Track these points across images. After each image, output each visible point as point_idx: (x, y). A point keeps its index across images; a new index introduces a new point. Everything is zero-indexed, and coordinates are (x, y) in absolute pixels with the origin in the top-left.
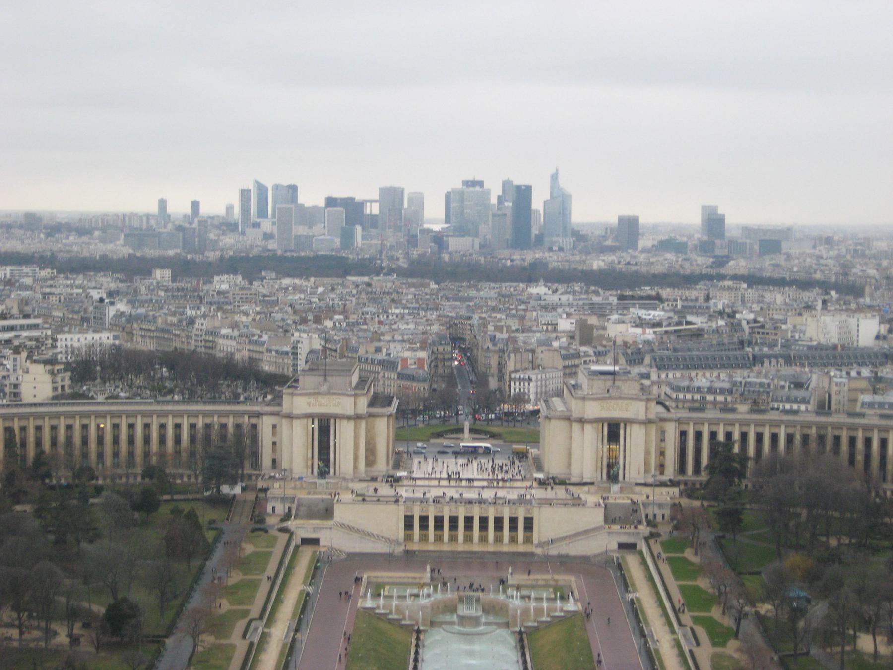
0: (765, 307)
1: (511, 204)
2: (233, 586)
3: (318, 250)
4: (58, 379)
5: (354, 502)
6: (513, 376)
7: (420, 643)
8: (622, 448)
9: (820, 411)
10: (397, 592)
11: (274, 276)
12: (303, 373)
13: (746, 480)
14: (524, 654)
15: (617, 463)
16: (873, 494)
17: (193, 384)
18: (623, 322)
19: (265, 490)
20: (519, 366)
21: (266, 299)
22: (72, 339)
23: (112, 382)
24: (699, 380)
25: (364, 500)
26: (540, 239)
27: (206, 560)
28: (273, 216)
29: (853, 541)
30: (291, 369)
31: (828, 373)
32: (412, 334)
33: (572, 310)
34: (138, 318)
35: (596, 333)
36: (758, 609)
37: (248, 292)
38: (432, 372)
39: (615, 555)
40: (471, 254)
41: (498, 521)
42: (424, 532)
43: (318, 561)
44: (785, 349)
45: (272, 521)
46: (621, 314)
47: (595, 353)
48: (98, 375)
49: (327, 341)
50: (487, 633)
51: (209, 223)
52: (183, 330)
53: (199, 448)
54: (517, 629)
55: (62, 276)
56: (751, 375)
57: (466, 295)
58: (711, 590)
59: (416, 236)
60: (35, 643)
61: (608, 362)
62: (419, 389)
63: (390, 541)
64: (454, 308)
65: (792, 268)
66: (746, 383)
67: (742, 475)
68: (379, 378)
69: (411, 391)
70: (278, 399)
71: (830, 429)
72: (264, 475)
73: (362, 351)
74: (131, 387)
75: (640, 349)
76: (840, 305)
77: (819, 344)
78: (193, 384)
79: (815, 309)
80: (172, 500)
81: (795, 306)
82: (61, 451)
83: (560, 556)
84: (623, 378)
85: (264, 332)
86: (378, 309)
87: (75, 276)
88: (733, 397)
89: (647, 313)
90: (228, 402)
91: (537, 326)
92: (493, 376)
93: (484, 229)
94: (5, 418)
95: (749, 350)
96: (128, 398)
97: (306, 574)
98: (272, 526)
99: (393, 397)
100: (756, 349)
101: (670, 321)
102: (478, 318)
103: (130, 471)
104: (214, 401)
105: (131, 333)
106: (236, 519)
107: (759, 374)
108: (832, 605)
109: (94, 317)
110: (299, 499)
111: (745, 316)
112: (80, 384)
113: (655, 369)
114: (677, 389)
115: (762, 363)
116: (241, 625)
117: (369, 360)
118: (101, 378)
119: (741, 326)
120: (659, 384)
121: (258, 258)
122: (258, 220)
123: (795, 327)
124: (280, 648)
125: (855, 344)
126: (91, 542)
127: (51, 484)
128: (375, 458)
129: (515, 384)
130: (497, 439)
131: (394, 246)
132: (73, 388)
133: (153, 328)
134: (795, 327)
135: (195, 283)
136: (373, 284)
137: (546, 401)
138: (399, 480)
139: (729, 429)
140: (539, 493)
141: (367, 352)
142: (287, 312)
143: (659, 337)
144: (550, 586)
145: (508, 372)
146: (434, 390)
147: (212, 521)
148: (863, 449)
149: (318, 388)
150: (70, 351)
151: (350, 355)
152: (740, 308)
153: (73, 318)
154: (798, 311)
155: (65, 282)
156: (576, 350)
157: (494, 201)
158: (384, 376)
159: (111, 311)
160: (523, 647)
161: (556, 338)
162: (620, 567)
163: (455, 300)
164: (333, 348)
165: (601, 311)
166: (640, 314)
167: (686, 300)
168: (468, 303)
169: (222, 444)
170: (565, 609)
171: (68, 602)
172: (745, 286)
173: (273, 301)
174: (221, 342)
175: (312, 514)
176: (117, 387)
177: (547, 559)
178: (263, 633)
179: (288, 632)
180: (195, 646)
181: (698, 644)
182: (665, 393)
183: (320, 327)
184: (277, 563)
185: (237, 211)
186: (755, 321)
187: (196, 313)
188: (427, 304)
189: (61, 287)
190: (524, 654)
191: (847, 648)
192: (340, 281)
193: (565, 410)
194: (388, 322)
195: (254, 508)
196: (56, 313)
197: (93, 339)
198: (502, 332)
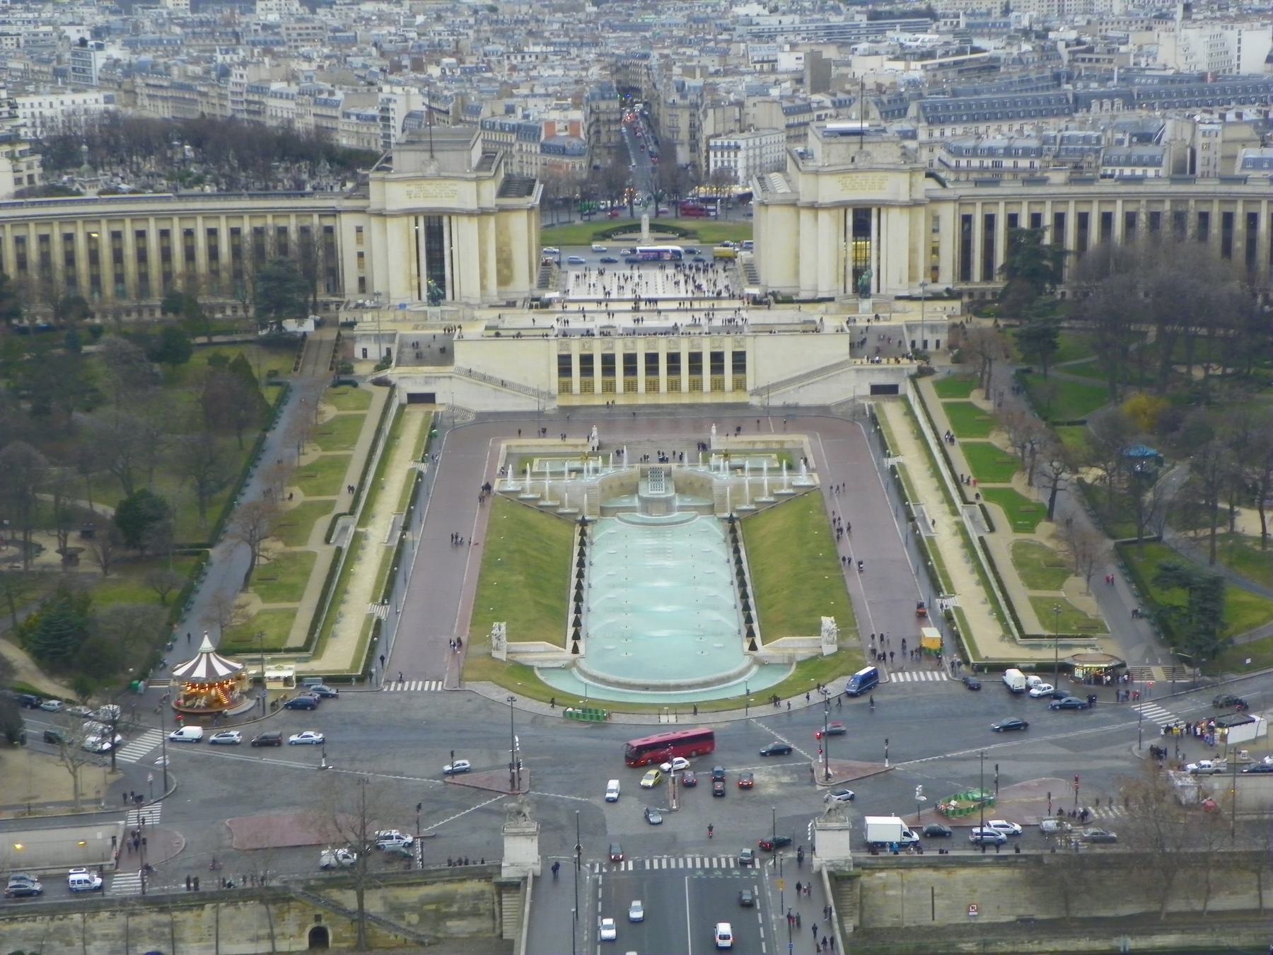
0: (1095, 19)
2: (309, 467)
4: (23, 166)
5: (483, 338)
6: (712, 142)
8: (874, 244)
9: (1177, 176)
10: (550, 468)
12: (397, 147)
13: (1062, 286)
14: (737, 551)
15: (867, 267)
16: (1260, 300)
17: (232, 169)
18: (877, 54)
20: (720, 128)
21: (337, 34)
22: (40, 104)
23: (107, 168)
24: (991, 137)
25: (498, 335)
27: (266, 430)
29: (1229, 371)
30: (381, 142)
31: (1192, 116)
32: (560, 85)
33: (799, 38)
34: (141, 68)
35: (835, 72)
36: (1083, 476)
37: (309, 25)
38: (592, 142)
39: (867, 403)
41: (695, 359)
42: (587, 379)
43: (433, 427)
44: (1124, 84)
45: (362, 369)
46: (872, 42)
47: (834, 103)
48: (85, 158)
49: (433, 98)
50: (682, 522)
52: (212, 86)
53: (248, 265)
54: (727, 515)
55: (19, 6)
56: (1071, 125)
57: (640, 20)
58: (1010, 450)
60: (9, 564)
61: (854, 117)
62: (574, 167)
63: (538, 394)
64: (622, 41)
67: (1056, 278)
68: (514, 152)
69: (561, 171)
71: (1192, 203)
72: (348, 303)
73: (485, 113)
74: (137, 175)
75: (901, 94)
76: (1212, 11)
77: (1178, 73)
78: (232, 169)
79: (1172, 19)
80: (210, 344)
81: (1142, 16)
82: (34, 275)
83: (786, 407)
84: (875, 139)
85: (337, 86)
86: (508, 46)
87: (40, 6)
88: (1043, 161)
89: (913, 37)
90: (288, 195)
91: (747, 66)
92: (682, 144)
95: (1068, 87)
96: (133, 192)
97: (416, 447)
98: (363, 378)
99: (534, 181)
100: (1080, 85)
101: (946, 48)
102: (658, 57)
103: (143, 303)
104: (265, 193)
105: (132, 92)
106: (309, 369)
107: (1083, 123)
108: (1195, 467)
109: (74, 69)
110: (402, 336)
111: (1063, 34)
112: (57, 172)
113: (924, 124)
114: (957, 152)
115: (1089, 108)
116: (322, 523)
117: (497, 127)
118: (90, 163)
119: (1056, 50)
120: (931, 146)
123: (1140, 47)
124: (381, 555)
125: (1235, 71)
126: (88, 410)
127: (21, 325)
128: (512, 272)
129: (715, 156)
130: (689, 238)
132: (48, 179)
133: (165, 84)
134: (1140, 47)
135: (227, 12)
136: (500, 7)
137: (761, 179)
138: (546, 304)
140: (757, 316)
141: (493, 114)
142: (370, 55)
143: (930, 73)
144: (773, 451)
145: (704, 137)
146: (596, 168)
147: (273, 374)
148: (1245, 230)
149: (421, 171)
150: (38, 122)
151: (468, 119)
152: (1055, 23)
153: (40, 72)
154: (1146, 23)
155: (24, 15)
156: (805, 99)
158: (521, 150)
159: (99, 60)
160: (735, 540)
162: (874, 420)
163: (623, 29)
164: (443, 108)
165: (842, 37)
166: (902, 40)
169: (282, 257)
170: (794, 483)
171: (57, 500)
173: (348, 37)
174: (272, 102)
175: (420, 354)
176: (116, 175)
177: (768, 410)
178: (356, 534)
179: (392, 531)
180: (254, 556)
181: (992, 529)
182: (940, 160)
183: (422, 76)
184: (374, 428)
186: (1079, 42)
187: (232, 59)
188: (581, 37)
189: (19, 23)
190: (737, 551)
191: (1220, 530)
193: (789, 191)
194: (523, 66)
195: (335, 351)
196: (13, 64)
197: (73, 102)
198: (694, 78)
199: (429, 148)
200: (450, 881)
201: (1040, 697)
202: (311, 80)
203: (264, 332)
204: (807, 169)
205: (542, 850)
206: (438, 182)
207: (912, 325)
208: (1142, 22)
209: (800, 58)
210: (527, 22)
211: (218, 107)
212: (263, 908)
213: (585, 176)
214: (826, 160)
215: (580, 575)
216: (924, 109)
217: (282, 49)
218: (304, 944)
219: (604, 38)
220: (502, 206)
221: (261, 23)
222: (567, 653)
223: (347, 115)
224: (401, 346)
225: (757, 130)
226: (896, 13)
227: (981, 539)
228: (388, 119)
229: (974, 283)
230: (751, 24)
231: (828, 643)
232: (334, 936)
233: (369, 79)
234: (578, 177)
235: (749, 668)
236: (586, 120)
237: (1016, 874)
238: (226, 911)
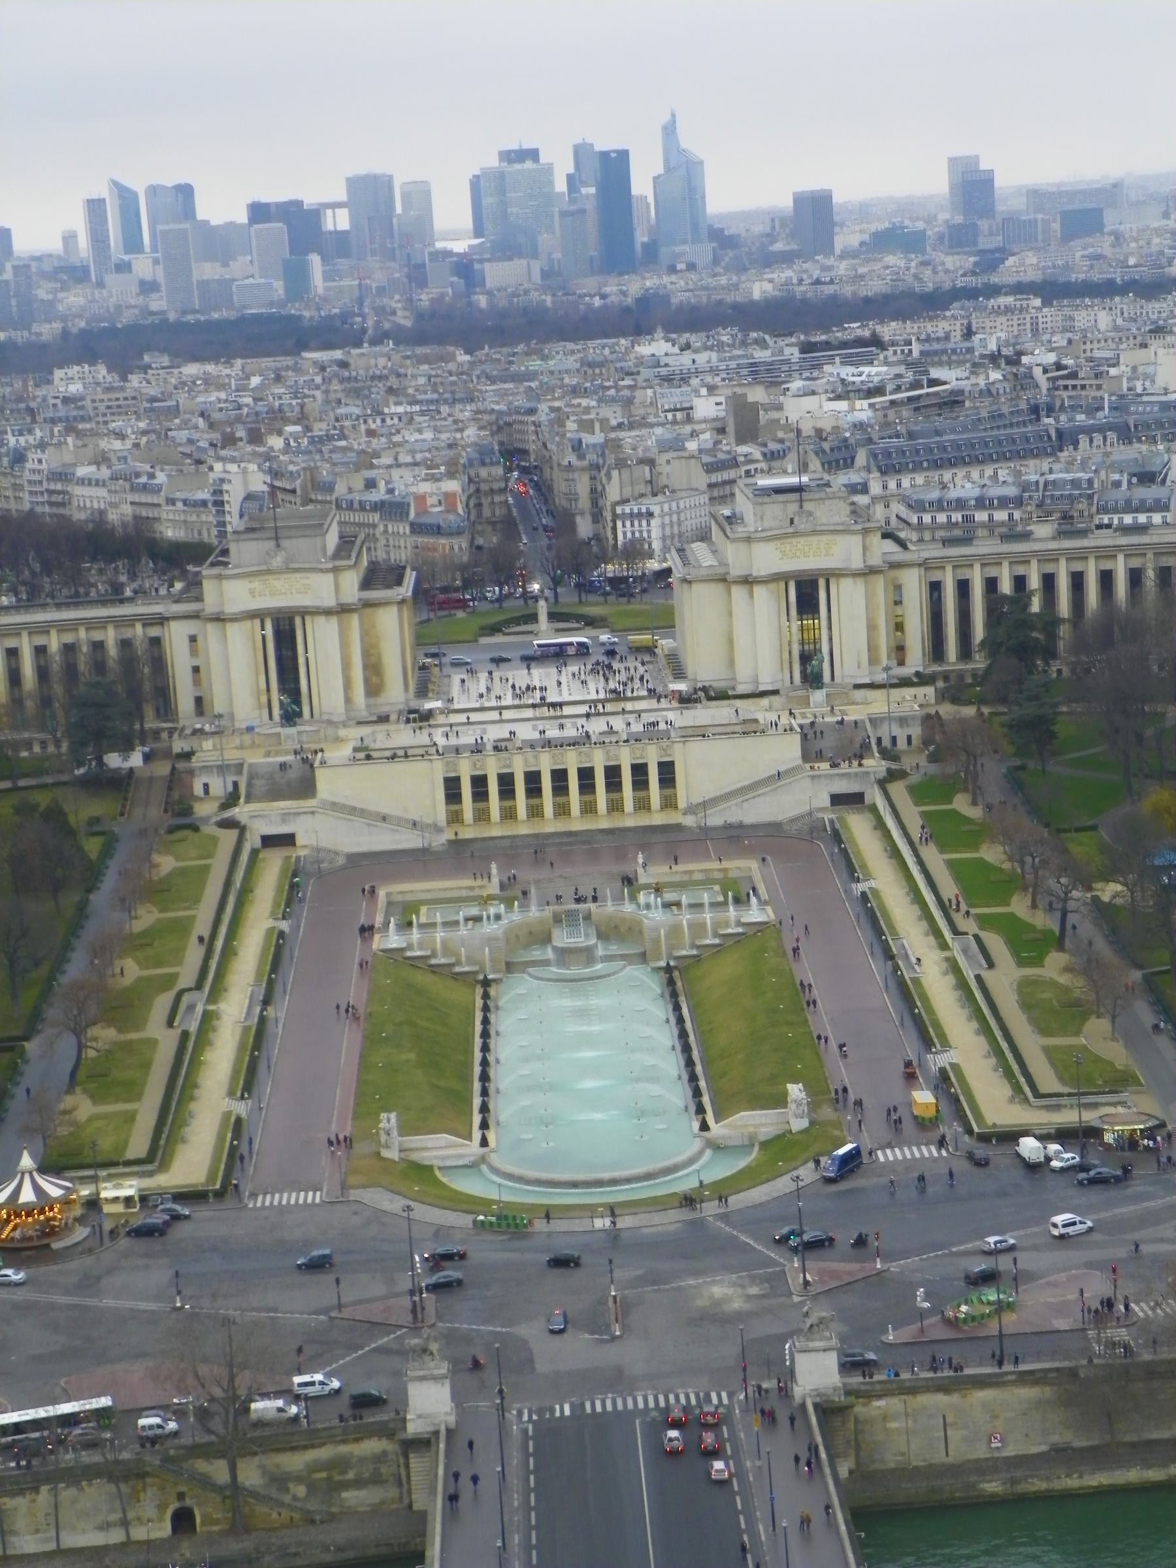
1: (592, 190)
3: (245, 307)
6: (619, 510)
7: (491, 1004)
8: (824, 623)
11: (165, 360)
14: (677, 1008)
18: (813, 393)
19: (187, 756)
20: (627, 492)
21: (155, 404)
25: (368, 757)
26: (651, 250)
28: (154, 248)
30: (215, 532)
32: (429, 451)
35: (763, 417)
37: (117, 395)
38: (472, 517)
39: (827, 817)
40: (526, 292)
41: (613, 773)
45: (204, 809)
46: (808, 379)
47: (764, 455)
49: (276, 474)
51: (34, 270)
53: (58, 689)
56: (1056, 467)
57: (523, 368)
59: (423, 265)
62: (452, 548)
64: (504, 394)
65: (1126, 260)
66: (1046, 483)
67: (1050, 653)
68: (378, 535)
70: (194, 587)
72: (183, 729)
73: (340, 489)
80: (16, 789)
84: (817, 496)
85: (158, 467)
92: (582, 514)
93: (548, 241)
94: (15, 631)
98: (206, 820)
99: (404, 568)
102: (547, 410)
106: (138, 812)
110: (251, 765)
111: (1039, 358)
113: (876, 474)
114: (918, 506)
115: (1076, 444)
116: (170, 996)
117: (356, 505)
120: (886, 501)
121: (134, 330)
122: (126, 258)
129: (624, 526)
131: (384, 288)
135: (18, 385)
136: (351, 361)
139: (1020, 570)
141: (350, 490)
142: (196, 427)
147: (96, 820)
149: (265, 563)
151: (319, 498)
152: (1028, 346)
156: (729, 452)
157: (561, 186)
158: (386, 531)
160: (674, 995)
161: (692, 435)
164: (288, 487)
167: (928, 339)
168: (527, 384)
172: (1037, 302)
174: (78, 491)
181: (991, 965)
183: (261, 449)
185: (83, 242)
188: (453, 392)
192: (289, 361)
193: (716, 564)
194: (385, 431)
199: (273, 535)
200: (344, 1442)
201: (1063, 1170)
202: (126, 462)
203: (82, 771)
204: (736, 536)
205: (455, 1396)
206: (286, 576)
207: (876, 719)
208: (1135, 338)
209: (721, 404)
210: (386, 377)
211: (12, 500)
212: (112, 1488)
213: (465, 559)
214: (759, 524)
215: (485, 1048)
216: (875, 456)
217: (88, 426)
218: (164, 1529)
219: (481, 391)
220: (367, 600)
221: (61, 395)
222: (473, 1147)
223: (171, 501)
224: (251, 777)
225: (673, 492)
226: (833, 343)
227: (978, 978)
228: (222, 503)
229: (949, 663)
230: (658, 365)
231: (796, 1116)
232: (203, 1516)
233: (196, 456)
234: (456, 561)
235: (701, 1153)
236: (463, 491)
237: (1047, 1391)
238: (67, 1493)
